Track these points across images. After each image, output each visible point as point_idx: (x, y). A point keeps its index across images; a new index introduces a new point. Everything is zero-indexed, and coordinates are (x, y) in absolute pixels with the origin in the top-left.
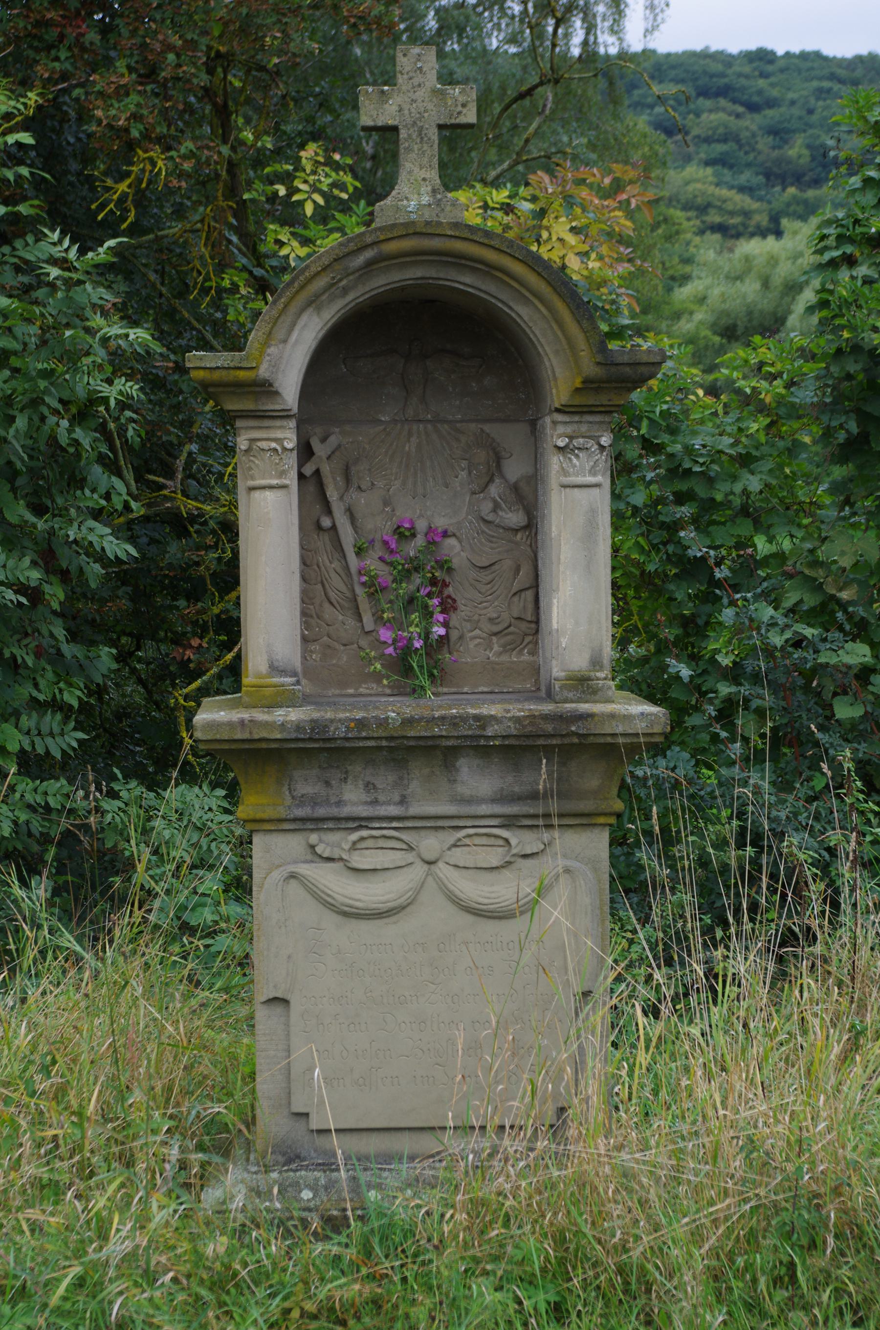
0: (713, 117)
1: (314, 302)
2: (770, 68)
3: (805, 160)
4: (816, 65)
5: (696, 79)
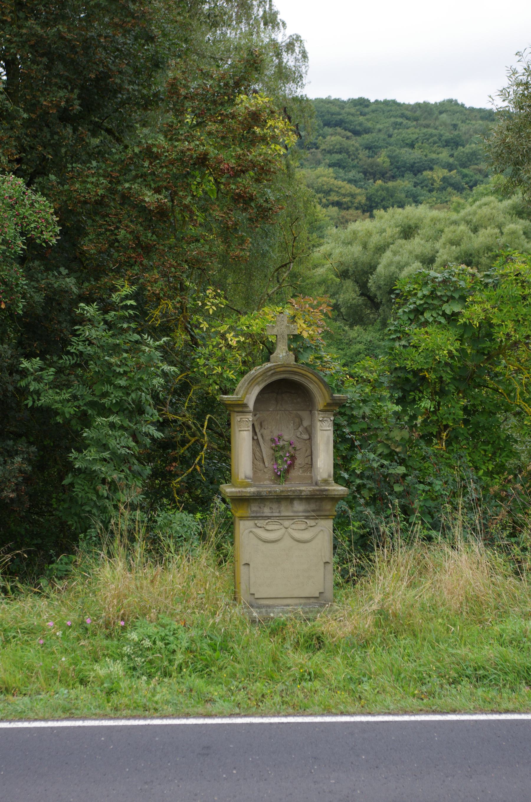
0: (333, 138)
1: (258, 384)
2: (366, 110)
3: (387, 164)
4: (393, 108)
5: (323, 116)
